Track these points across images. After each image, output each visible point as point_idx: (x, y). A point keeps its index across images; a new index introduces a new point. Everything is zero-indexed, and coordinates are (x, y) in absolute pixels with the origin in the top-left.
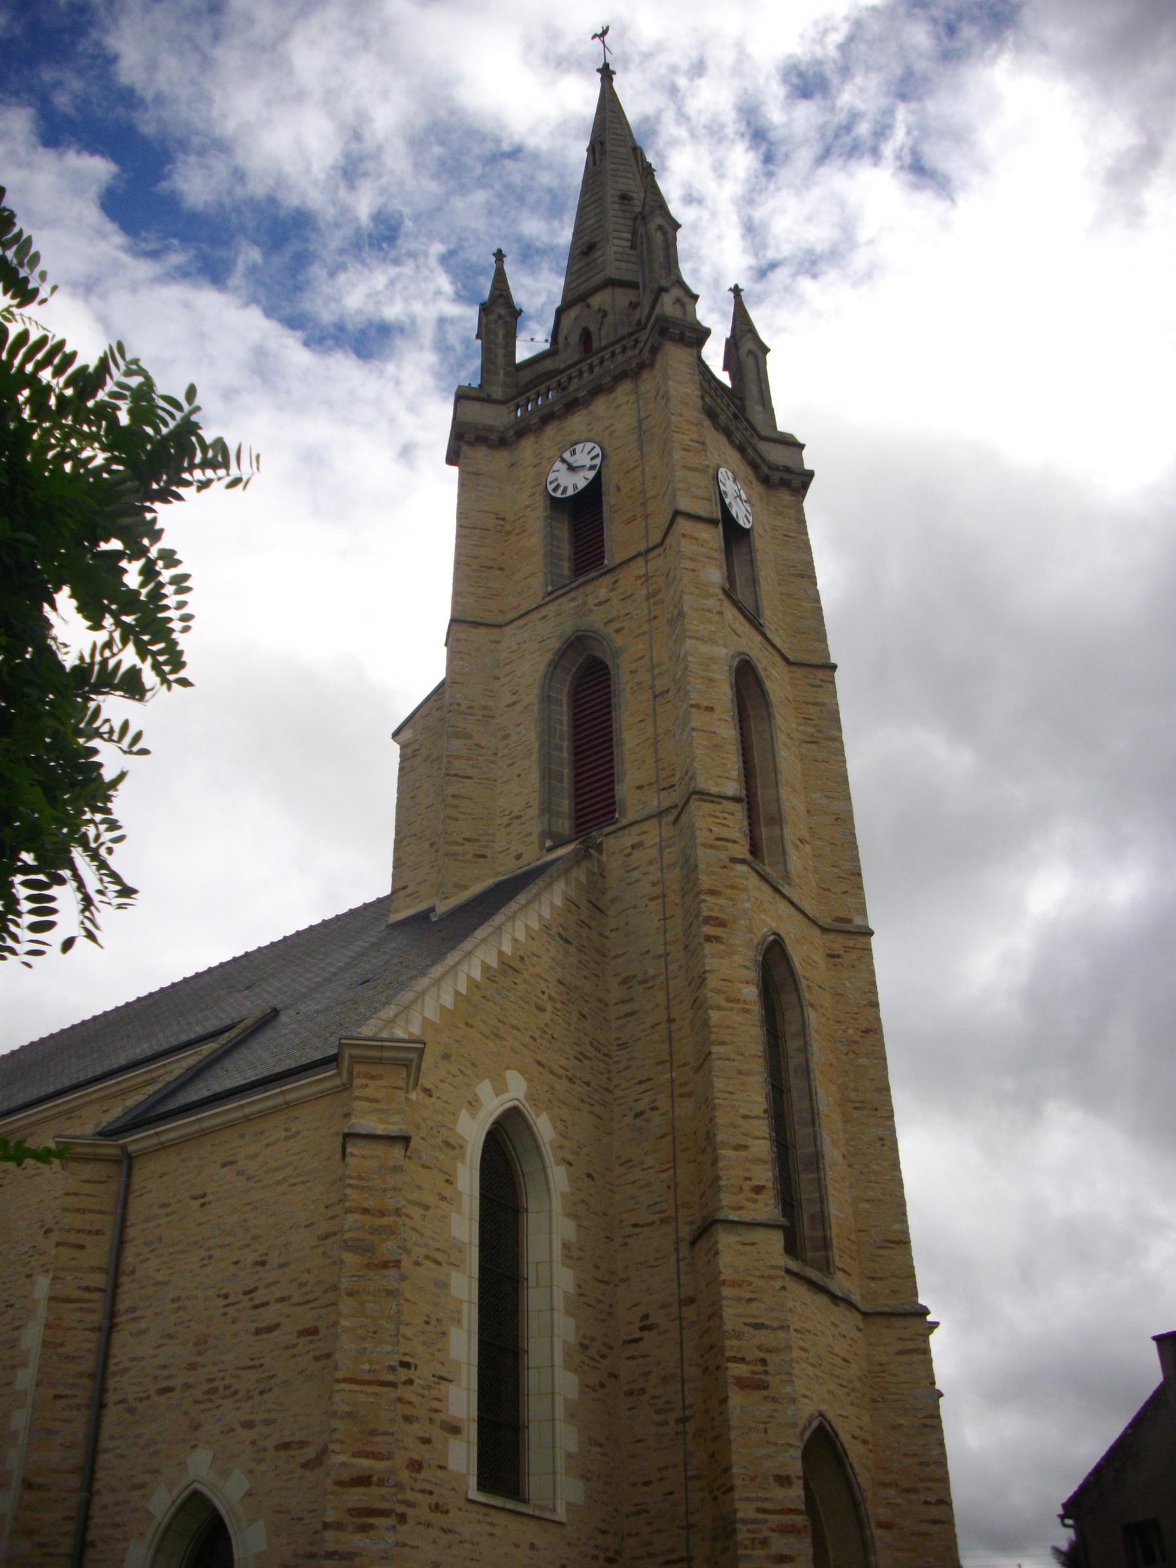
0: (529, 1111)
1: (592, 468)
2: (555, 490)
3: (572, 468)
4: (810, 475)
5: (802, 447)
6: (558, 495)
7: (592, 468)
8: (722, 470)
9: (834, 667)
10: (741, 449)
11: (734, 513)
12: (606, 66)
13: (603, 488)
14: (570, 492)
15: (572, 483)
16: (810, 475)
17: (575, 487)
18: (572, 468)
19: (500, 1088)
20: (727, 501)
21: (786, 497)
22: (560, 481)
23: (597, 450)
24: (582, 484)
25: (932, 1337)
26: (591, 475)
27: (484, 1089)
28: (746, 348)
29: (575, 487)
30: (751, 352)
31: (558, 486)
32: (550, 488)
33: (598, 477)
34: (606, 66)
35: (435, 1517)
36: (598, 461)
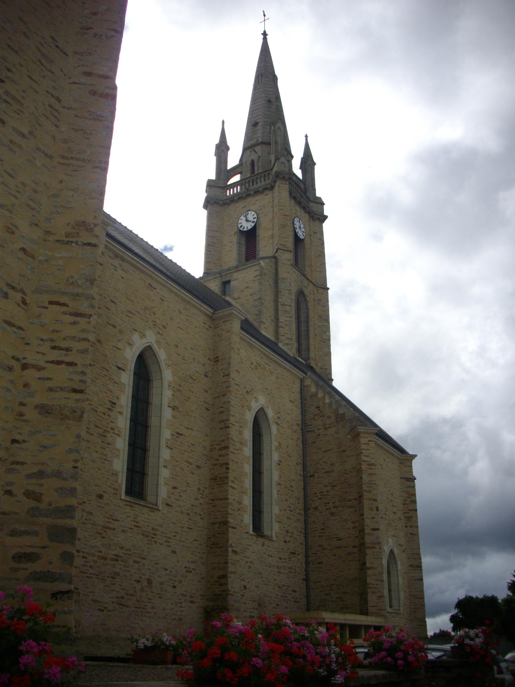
0: (155, 347)
1: (253, 222)
2: (241, 227)
3: (247, 220)
4: (326, 217)
5: (324, 204)
6: (241, 229)
7: (253, 222)
8: (296, 219)
9: (328, 289)
10: (304, 208)
11: (299, 235)
12: (265, 32)
13: (257, 239)
14: (245, 229)
15: (248, 226)
16: (326, 217)
17: (247, 228)
18: (247, 220)
19: (143, 336)
20: (297, 231)
21: (317, 222)
22: (242, 224)
23: (255, 216)
24: (250, 228)
25: (413, 461)
26: (253, 224)
27: (136, 337)
28: (308, 162)
29: (247, 228)
30: (310, 165)
31: (242, 226)
32: (239, 226)
33: (255, 226)
34: (265, 32)
35: (85, 555)
36: (255, 220)
